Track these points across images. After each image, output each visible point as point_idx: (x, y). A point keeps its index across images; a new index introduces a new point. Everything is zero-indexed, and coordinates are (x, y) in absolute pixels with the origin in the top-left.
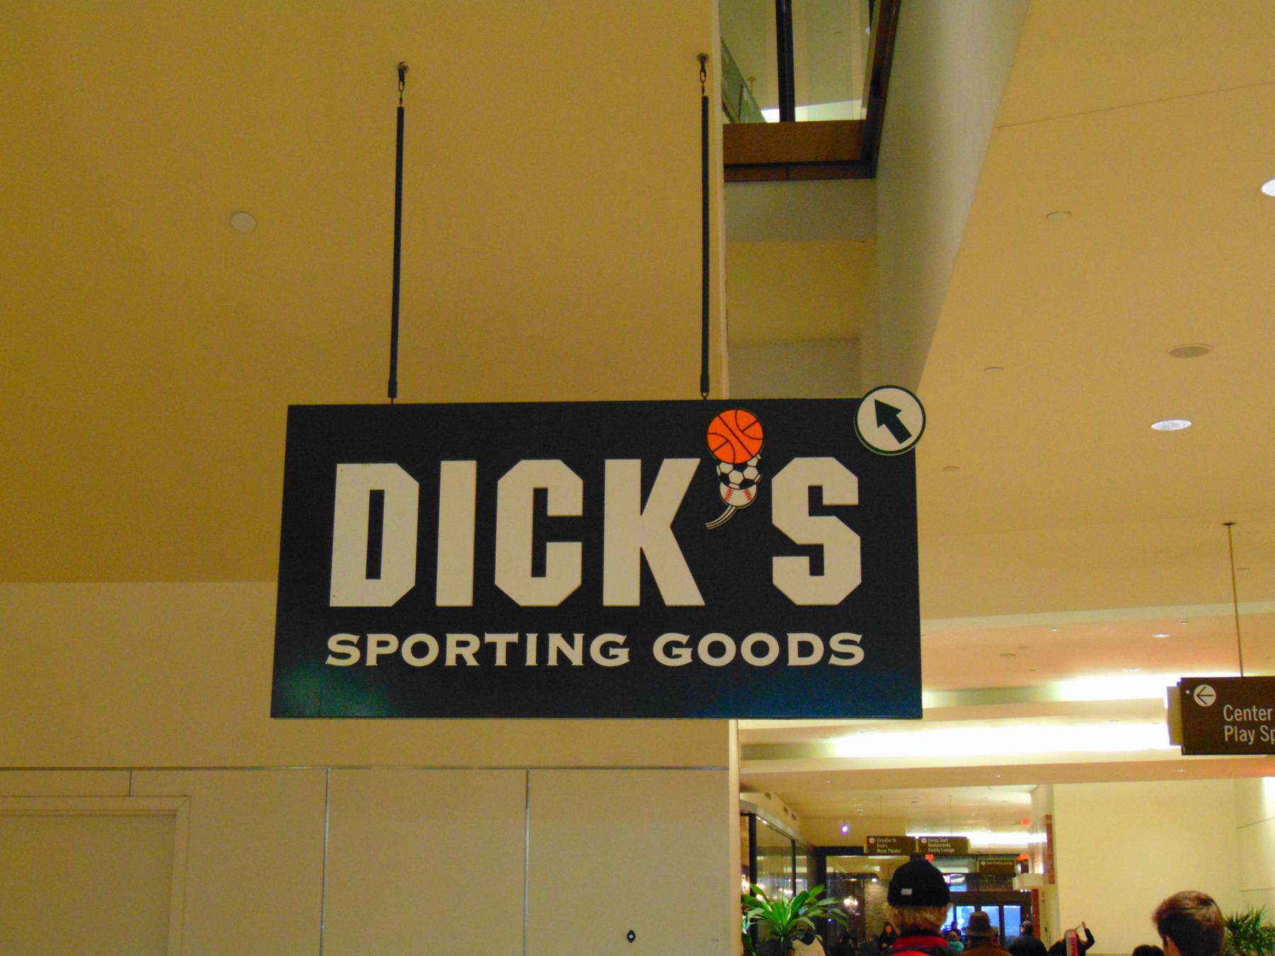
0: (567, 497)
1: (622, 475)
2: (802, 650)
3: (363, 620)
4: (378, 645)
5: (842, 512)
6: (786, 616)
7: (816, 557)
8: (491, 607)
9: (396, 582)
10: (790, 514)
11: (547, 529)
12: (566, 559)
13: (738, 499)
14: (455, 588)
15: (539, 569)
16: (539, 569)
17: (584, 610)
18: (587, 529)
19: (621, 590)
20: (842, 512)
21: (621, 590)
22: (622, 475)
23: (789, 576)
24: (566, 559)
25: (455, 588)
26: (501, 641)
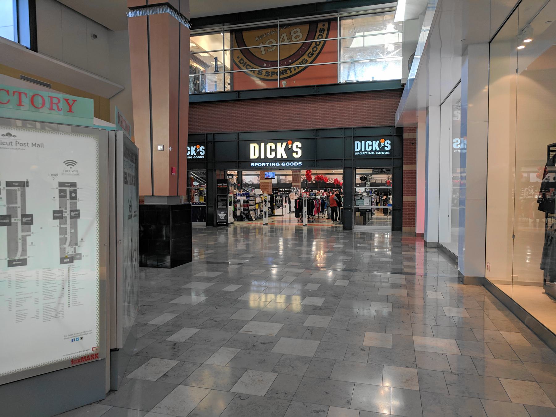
0: (371, 143)
1: (279, 144)
2: (296, 164)
3: (357, 152)
4: (358, 153)
5: (300, 148)
6: (385, 151)
7: (297, 153)
8: (366, 151)
9: (257, 156)
10: (294, 148)
11: (369, 146)
12: (370, 147)
13: (290, 147)
14: (363, 150)
15: (271, 154)
16: (271, 154)
17: (372, 151)
18: (372, 146)
19: (374, 149)
20: (300, 148)
21: (374, 149)
22: (279, 144)
23: (294, 155)
24: (273, 153)
25: (363, 150)
26: (267, 164)
